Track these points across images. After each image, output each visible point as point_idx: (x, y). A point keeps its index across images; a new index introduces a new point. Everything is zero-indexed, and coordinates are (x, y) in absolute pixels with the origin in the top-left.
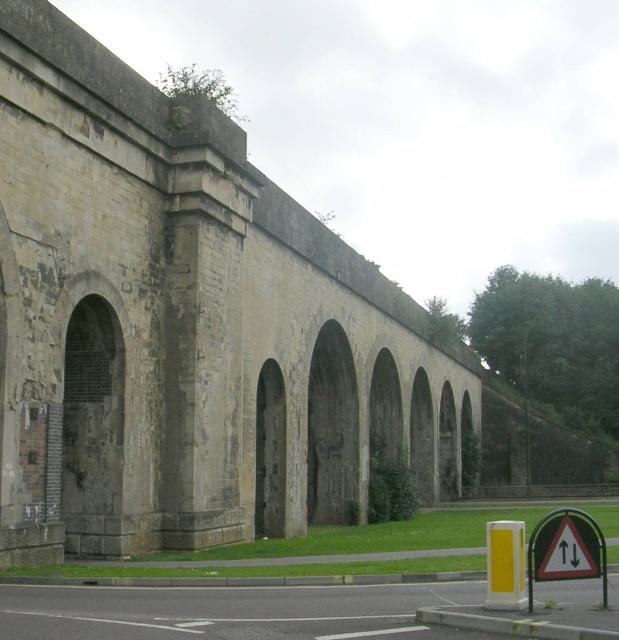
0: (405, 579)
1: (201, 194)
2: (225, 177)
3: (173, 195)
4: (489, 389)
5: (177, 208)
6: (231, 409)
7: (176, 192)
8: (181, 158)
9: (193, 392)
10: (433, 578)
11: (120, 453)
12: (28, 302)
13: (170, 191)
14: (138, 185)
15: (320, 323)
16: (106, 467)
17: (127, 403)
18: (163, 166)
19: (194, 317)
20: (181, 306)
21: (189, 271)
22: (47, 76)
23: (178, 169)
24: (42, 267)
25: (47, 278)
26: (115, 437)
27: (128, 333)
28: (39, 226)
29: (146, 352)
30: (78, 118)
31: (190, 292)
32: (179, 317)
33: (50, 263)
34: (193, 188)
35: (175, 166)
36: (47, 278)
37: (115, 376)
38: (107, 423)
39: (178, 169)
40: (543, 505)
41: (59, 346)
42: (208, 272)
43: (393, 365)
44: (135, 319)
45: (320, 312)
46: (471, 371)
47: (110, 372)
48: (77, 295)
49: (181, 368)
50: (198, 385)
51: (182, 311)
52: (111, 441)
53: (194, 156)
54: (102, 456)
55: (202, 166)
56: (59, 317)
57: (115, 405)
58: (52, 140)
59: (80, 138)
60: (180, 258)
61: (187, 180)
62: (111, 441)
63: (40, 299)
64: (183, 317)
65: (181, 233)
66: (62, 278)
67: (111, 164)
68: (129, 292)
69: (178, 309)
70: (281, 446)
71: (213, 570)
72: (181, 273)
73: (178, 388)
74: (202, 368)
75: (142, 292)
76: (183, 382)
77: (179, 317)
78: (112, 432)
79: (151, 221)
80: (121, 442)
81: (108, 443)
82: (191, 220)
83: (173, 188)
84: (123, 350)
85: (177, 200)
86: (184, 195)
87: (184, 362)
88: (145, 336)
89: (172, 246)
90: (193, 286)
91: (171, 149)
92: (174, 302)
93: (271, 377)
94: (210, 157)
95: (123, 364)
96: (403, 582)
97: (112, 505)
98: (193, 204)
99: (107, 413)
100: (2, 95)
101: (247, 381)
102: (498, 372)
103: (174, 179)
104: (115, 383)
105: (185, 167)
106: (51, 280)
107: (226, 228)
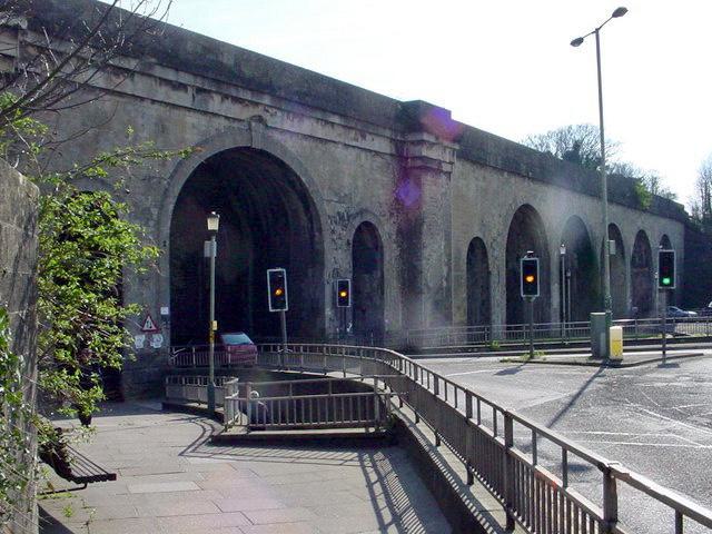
1: (422, 158)
6: (445, 274)
9: (421, 265)
11: (382, 299)
12: (333, 232)
15: (515, 208)
17: (385, 273)
19: (421, 225)
24: (339, 213)
25: (342, 218)
27: (384, 239)
28: (336, 194)
29: (395, 246)
33: (342, 210)
34: (417, 154)
36: (342, 218)
38: (375, 285)
42: (428, 199)
43: (646, 238)
44: (387, 230)
45: (515, 201)
46: (671, 218)
48: (357, 223)
50: (424, 262)
53: (418, 137)
55: (422, 142)
56: (349, 235)
57: (379, 275)
59: (354, 143)
61: (415, 150)
63: (338, 229)
66: (348, 217)
67: (370, 151)
68: (384, 216)
70: (487, 288)
71: (496, 486)
74: (426, 252)
75: (392, 214)
80: (383, 293)
82: (416, 172)
84: (382, 247)
86: (414, 158)
88: (394, 237)
91: (403, 134)
93: (477, 248)
94: (425, 137)
95: (382, 255)
98: (419, 163)
100: (709, 531)
101: (458, 258)
104: (379, 265)
106: (342, 219)
107: (439, 171)
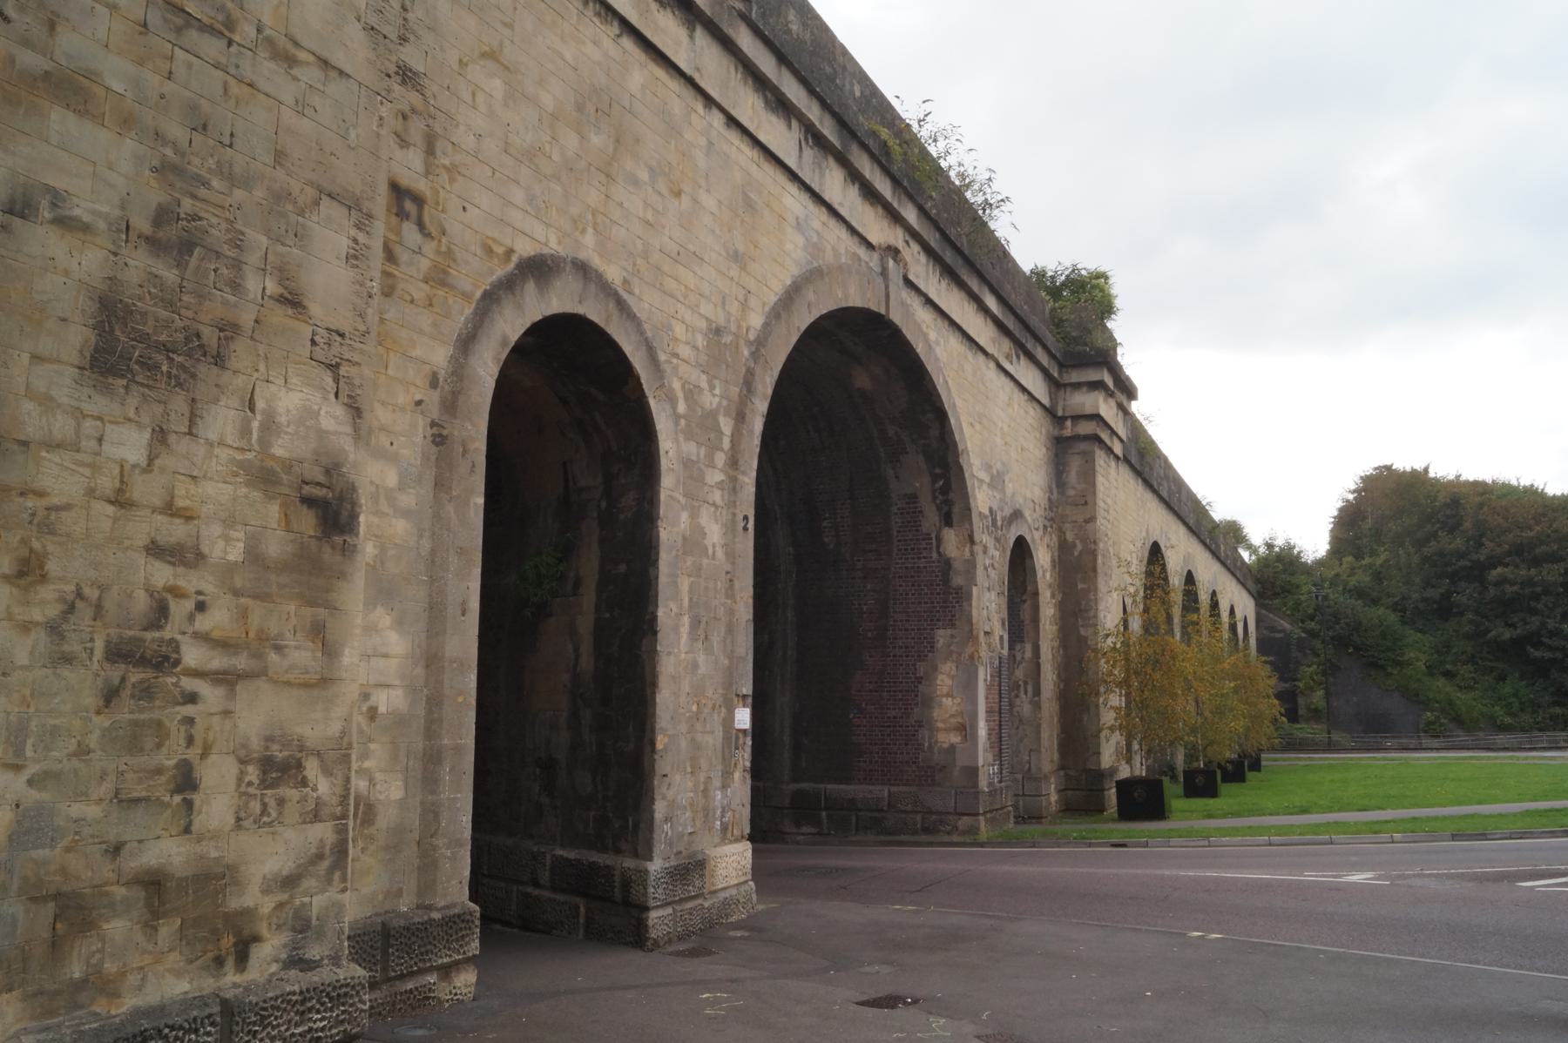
0: (1454, 837)
1: (1097, 417)
2: (1112, 395)
3: (1064, 418)
4: (1263, 612)
5: (1068, 432)
7: (1067, 415)
8: (1075, 376)
10: (1483, 836)
13: (1060, 414)
14: (1039, 409)
16: (1021, 721)
18: (1055, 385)
20: (1077, 542)
21: (1086, 503)
22: (991, 302)
23: (1068, 390)
26: (1030, 688)
30: (1007, 345)
31: (1089, 526)
32: (1076, 554)
34: (1089, 410)
35: (1065, 386)
37: (1027, 622)
39: (1068, 390)
40: (1305, 759)
41: (1003, 593)
47: (1022, 617)
49: (1080, 610)
51: (1079, 547)
52: (1026, 693)
53: (1092, 375)
54: (1015, 709)
55: (1098, 385)
57: (1028, 654)
58: (991, 372)
60: (1074, 488)
62: (1026, 693)
64: (1081, 552)
65: (1075, 464)
69: (1074, 546)
72: (1077, 505)
73: (1079, 632)
76: (1082, 626)
77: (1076, 554)
78: (1026, 683)
79: (1048, 449)
81: (1022, 695)
82: (1083, 446)
83: (1064, 410)
85: (1069, 423)
86: (1077, 418)
87: (1083, 603)
89: (1065, 475)
90: (1092, 519)
91: (1062, 366)
92: (1070, 537)
96: (1453, 840)
97: (1030, 763)
98: (1086, 428)
99: (1020, 663)
102: (917, 485)
103: (1065, 400)
105: (1077, 386)
